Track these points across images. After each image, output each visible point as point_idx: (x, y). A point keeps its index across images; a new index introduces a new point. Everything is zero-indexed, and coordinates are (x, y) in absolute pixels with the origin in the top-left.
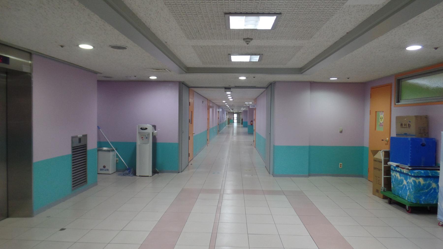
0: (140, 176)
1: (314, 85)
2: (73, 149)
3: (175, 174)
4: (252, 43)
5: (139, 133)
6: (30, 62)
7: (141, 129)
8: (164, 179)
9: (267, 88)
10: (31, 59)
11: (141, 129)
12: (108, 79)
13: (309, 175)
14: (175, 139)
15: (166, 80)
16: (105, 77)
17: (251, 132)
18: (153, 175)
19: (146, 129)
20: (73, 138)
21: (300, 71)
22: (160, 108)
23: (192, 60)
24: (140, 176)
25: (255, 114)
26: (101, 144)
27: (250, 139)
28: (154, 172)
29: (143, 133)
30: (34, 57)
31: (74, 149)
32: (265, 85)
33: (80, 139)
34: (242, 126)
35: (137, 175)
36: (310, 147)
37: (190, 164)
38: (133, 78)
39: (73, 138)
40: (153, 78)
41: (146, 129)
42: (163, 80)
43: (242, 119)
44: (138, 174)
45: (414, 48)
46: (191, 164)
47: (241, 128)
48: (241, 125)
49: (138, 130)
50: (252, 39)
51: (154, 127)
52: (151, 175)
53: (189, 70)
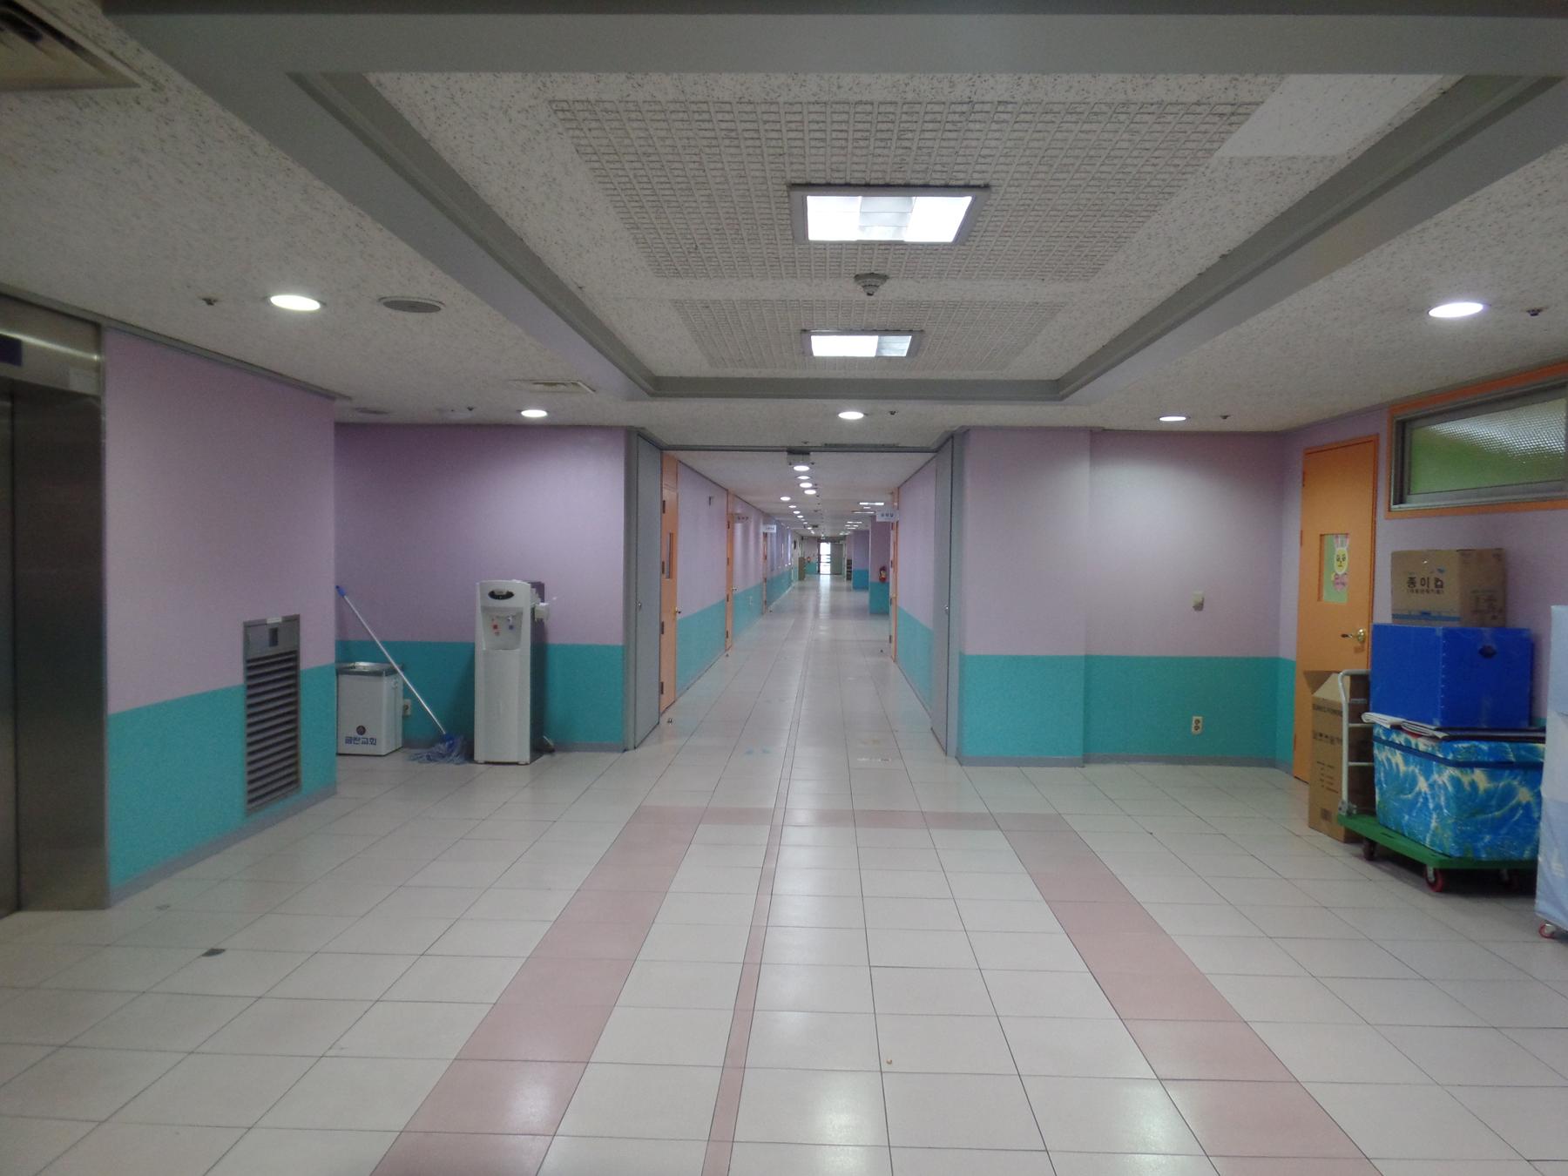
1: (1105, 442)
2: (249, 669)
3: (613, 757)
4: (887, 291)
5: (485, 609)
6: (95, 357)
7: (493, 595)
10: (98, 348)
11: (493, 595)
12: (372, 418)
14: (613, 634)
19: (510, 595)
20: (248, 626)
22: (558, 522)
23: (674, 352)
27: (878, 630)
28: (540, 748)
30: (110, 339)
31: (255, 668)
33: (274, 632)
38: (463, 416)
39: (248, 626)
40: (534, 414)
41: (510, 595)
43: (849, 562)
45: (1456, 310)
47: (845, 594)
48: (845, 584)
49: (480, 599)
50: (885, 278)
51: (539, 588)
53: (661, 387)
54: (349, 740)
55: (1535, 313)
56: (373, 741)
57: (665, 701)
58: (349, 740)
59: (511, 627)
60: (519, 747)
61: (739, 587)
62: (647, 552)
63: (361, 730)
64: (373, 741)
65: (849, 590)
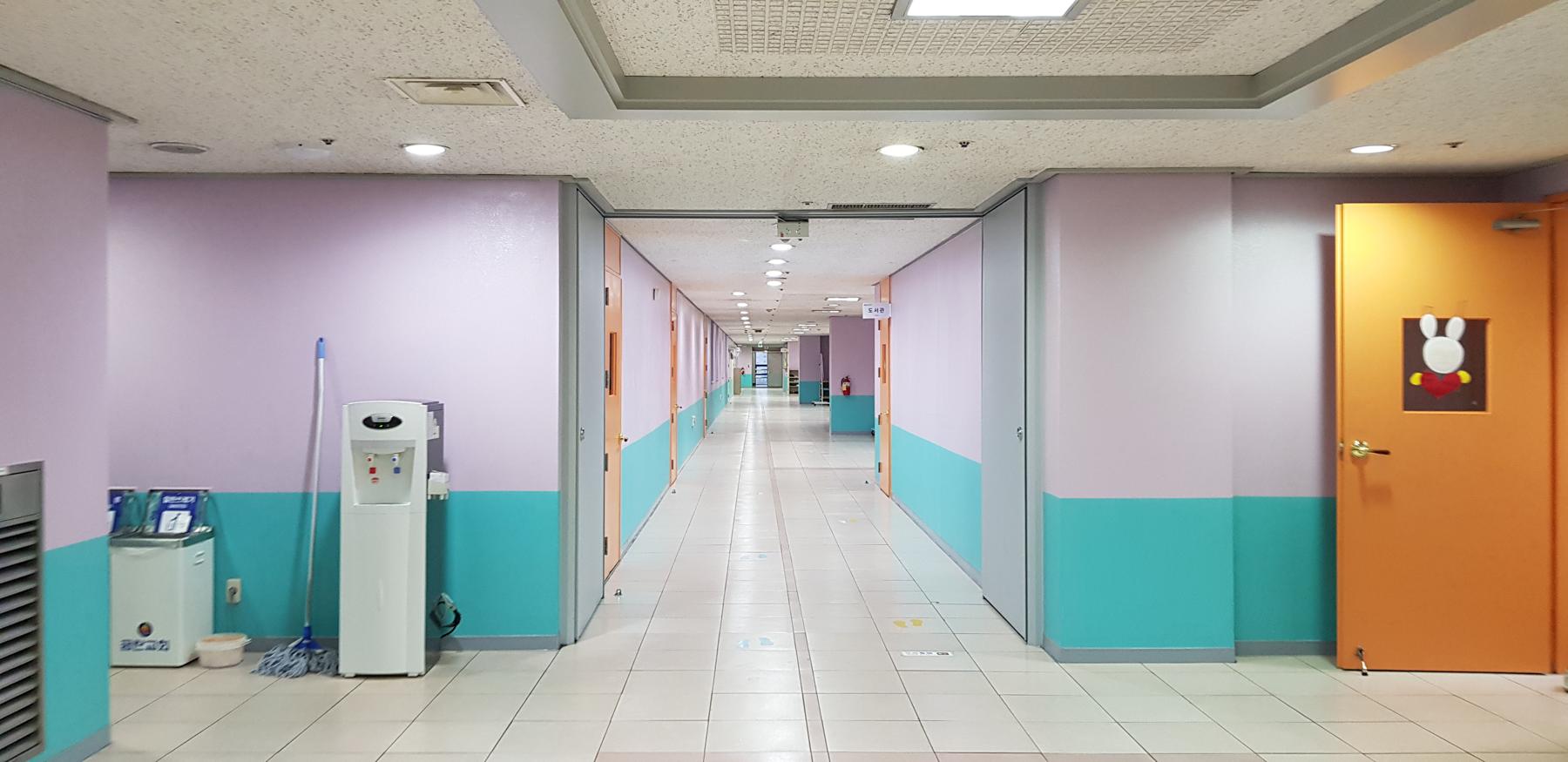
0: (357, 676)
3: (544, 657)
5: (356, 446)
7: (368, 422)
8: (484, 676)
9: (981, 215)
11: (368, 422)
12: (180, 163)
13: (1242, 650)
14: (553, 486)
15: (495, 164)
16: (164, 147)
17: (857, 420)
18: (430, 662)
19: (395, 422)
21: (1250, 90)
22: (459, 317)
24: (357, 676)
25: (885, 349)
26: (131, 519)
27: (858, 457)
28: (442, 630)
29: (375, 444)
32: (976, 198)
34: (796, 398)
35: (341, 671)
36: (1236, 500)
37: (610, 588)
38: (317, 157)
40: (424, 152)
41: (395, 422)
42: (475, 171)
43: (792, 373)
44: (349, 661)
46: (619, 594)
47: (788, 410)
48: (788, 398)
49: (352, 429)
51: (436, 409)
52: (422, 669)
54: (127, 646)
55: (1454, 145)
56: (164, 645)
57: (610, 559)
58: (127, 646)
59: (397, 470)
60: (404, 637)
61: (682, 401)
62: (588, 364)
63: (145, 630)
64: (164, 645)
65: (792, 404)
